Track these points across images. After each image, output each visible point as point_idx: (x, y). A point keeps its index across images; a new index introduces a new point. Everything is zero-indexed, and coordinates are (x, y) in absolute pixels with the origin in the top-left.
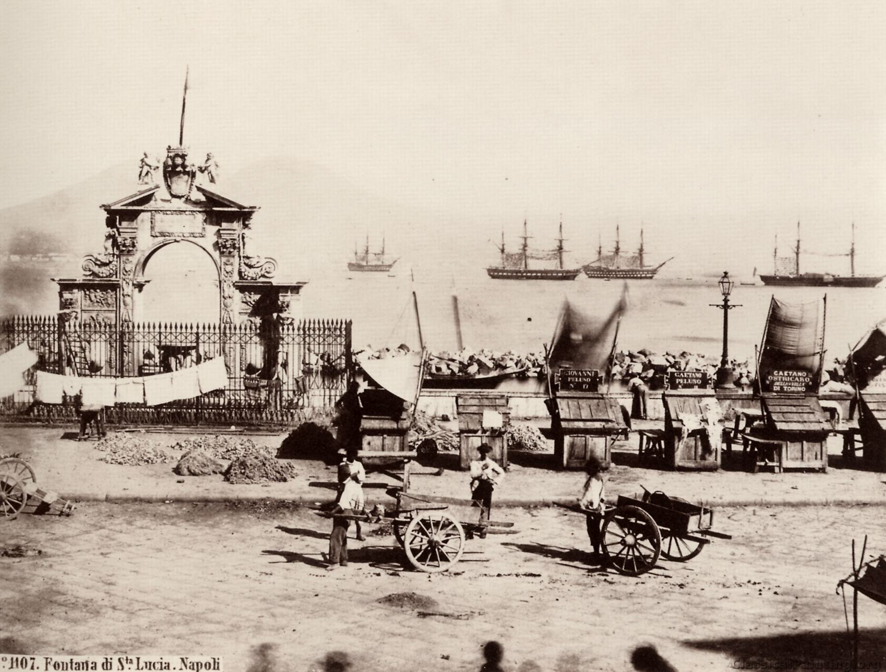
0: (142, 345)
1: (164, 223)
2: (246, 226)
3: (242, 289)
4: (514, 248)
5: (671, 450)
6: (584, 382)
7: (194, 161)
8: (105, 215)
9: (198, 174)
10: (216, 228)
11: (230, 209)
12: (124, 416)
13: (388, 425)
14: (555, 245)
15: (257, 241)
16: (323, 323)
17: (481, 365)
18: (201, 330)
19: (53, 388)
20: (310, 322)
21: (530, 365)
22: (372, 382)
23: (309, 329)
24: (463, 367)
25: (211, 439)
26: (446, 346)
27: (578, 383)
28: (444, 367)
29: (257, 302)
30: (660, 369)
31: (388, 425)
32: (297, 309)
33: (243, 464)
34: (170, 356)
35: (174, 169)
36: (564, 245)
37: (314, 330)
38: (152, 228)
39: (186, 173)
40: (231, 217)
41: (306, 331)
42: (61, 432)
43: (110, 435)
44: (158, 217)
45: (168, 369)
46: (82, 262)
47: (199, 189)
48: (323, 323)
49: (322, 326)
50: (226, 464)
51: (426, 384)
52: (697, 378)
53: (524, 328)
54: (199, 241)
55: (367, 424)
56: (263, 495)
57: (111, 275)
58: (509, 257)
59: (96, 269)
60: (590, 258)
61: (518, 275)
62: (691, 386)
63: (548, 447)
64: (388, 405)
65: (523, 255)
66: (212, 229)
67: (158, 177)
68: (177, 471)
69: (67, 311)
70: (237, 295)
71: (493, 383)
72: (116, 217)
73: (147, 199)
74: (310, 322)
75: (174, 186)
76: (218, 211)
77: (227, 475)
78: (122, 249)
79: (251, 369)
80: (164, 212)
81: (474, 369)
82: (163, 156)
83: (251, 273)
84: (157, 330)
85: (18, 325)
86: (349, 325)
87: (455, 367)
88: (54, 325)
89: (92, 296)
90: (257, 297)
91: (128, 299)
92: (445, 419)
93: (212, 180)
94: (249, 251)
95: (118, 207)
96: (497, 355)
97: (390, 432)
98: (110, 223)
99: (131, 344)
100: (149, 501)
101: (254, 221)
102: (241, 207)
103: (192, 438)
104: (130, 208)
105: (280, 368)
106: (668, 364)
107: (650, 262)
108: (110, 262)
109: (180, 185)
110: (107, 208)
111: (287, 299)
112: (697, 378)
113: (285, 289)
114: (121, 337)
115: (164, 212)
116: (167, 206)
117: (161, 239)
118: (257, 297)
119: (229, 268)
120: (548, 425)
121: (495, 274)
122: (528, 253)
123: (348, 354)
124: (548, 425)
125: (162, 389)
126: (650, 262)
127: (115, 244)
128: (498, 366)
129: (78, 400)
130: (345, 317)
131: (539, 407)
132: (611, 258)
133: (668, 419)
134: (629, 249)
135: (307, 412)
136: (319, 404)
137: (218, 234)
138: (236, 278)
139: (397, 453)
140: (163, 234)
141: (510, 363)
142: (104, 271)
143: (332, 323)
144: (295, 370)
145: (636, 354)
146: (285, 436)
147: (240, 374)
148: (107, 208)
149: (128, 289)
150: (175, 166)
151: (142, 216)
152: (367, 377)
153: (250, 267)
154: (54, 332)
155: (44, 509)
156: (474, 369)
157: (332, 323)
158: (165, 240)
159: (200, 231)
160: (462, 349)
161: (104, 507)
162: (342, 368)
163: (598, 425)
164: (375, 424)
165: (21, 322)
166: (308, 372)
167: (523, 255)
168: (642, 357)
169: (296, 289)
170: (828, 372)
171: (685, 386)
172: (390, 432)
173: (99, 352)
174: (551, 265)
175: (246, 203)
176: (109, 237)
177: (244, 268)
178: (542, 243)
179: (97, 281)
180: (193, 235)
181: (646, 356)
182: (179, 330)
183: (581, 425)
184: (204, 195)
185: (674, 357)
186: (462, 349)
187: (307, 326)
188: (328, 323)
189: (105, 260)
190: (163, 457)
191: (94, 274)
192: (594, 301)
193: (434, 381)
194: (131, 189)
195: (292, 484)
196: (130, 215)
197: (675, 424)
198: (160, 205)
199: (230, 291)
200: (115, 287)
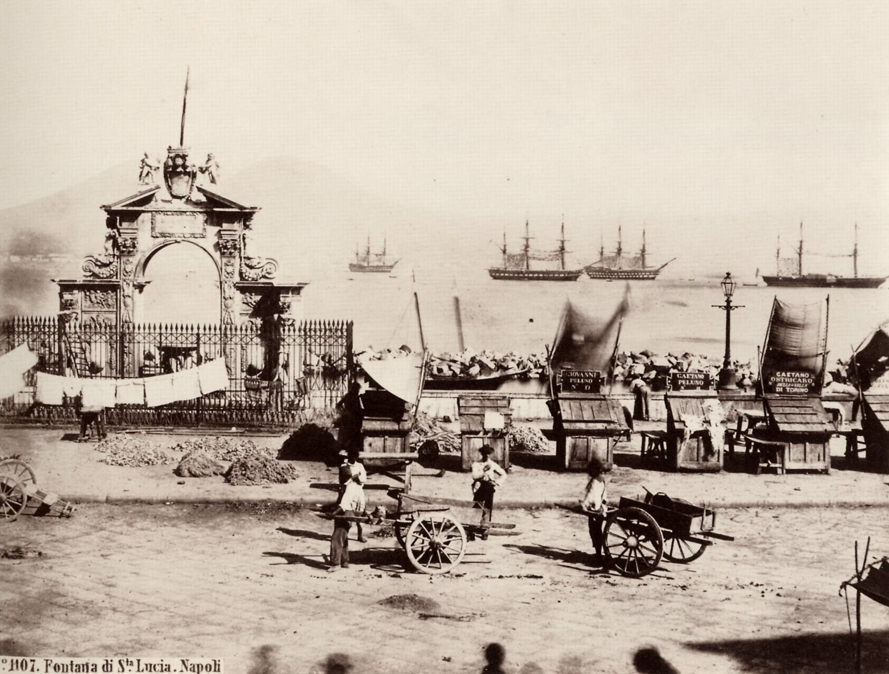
0: (143, 346)
1: (165, 224)
2: (247, 227)
3: (243, 290)
4: (516, 249)
5: (673, 451)
6: (586, 384)
7: (195, 161)
8: (105, 216)
9: (199, 174)
10: (216, 229)
11: (230, 210)
12: (124, 417)
13: (390, 426)
14: (557, 246)
15: (258, 242)
16: (324, 324)
17: (483, 366)
18: (201, 331)
19: (53, 389)
20: (311, 323)
21: (532, 366)
22: (373, 383)
23: (310, 330)
24: (465, 368)
25: (212, 440)
26: (447, 347)
27: (580, 384)
28: (445, 368)
29: (258, 303)
30: (662, 370)
31: (390, 426)
32: (298, 310)
33: (244, 466)
34: (171, 357)
35: (175, 169)
36: (566, 245)
37: (315, 331)
38: (153, 229)
39: (186, 173)
40: (231, 218)
41: (307, 332)
42: (62, 433)
43: (111, 436)
44: (159, 217)
45: (168, 370)
46: (82, 262)
47: (200, 190)
48: (324, 324)
49: (323, 327)
50: (226, 466)
51: (427, 385)
52: (699, 380)
53: (526, 329)
54: (200, 241)
55: (368, 425)
56: (264, 497)
57: (111, 276)
58: (511, 258)
59: (97, 270)
60: (592, 259)
61: (519, 276)
62: (693, 387)
63: (550, 448)
64: (389, 406)
65: (525, 255)
66: (213, 230)
67: (158, 178)
68: (178, 472)
69: (67, 312)
70: (238, 296)
71: (494, 384)
72: (116, 217)
73: (147, 200)
74: (311, 323)
75: (174, 187)
76: (219, 211)
77: (227, 477)
78: (123, 250)
79: (251, 370)
80: (165, 212)
81: (475, 370)
82: (164, 157)
83: (251, 274)
84: (158, 331)
85: (18, 326)
86: (350, 326)
87: (457, 369)
88: (54, 326)
89: (93, 296)
90: (258, 298)
91: (128, 300)
92: (447, 420)
93: (213, 181)
94: (250, 251)
95: (118, 207)
96: (499, 356)
97: (392, 434)
98: (111, 224)
99: (131, 345)
100: (150, 503)
101: (255, 222)
102: (241, 208)
103: (193, 439)
104: (131, 208)
105: (281, 369)
106: (670, 365)
107: (652, 262)
108: (111, 263)
109: (181, 186)
110: (107, 209)
111: (288, 300)
112: (699, 380)
113: (286, 290)
114: (121, 338)
115: (165, 212)
116: (167, 207)
117: (161, 240)
118: (258, 298)
119: (230, 269)
120: (550, 426)
121: (497, 274)
122: (530, 254)
123: (349, 355)
124: (550, 426)
125: (163, 390)
126: (652, 262)
127: (115, 245)
128: (500, 367)
129: (78, 401)
130: (347, 318)
131: (541, 408)
132: (613, 259)
133: (670, 420)
134: (631, 250)
135: (309, 413)
136: (320, 405)
137: (219, 234)
138: (237, 278)
139: (398, 455)
140: (163, 235)
141: (511, 365)
142: (105, 272)
143: (334, 324)
144: (296, 371)
145: (638, 355)
146: (286, 437)
147: (241, 375)
148: (107, 209)
149: (129, 290)
150: (175, 166)
151: (143, 217)
152: (368, 379)
153: (251, 267)
154: (54, 333)
155: (44, 510)
156: (475, 370)
157: (334, 324)
158: (166, 240)
159: (201, 231)
160: (463, 350)
161: (105, 509)
162: (343, 369)
163: (600, 426)
164: (376, 425)
165: (21, 323)
166: (309, 373)
167: (525, 255)
168: (645, 358)
169: (297, 290)
170: (831, 373)
171: (688, 387)
172: (392, 434)
173: (100, 353)
174: (553, 266)
175: (247, 204)
176: (109, 237)
177: (245, 269)
178: (544, 244)
179: (97, 282)
180: (193, 235)
181: (648, 357)
182: (179, 331)
183: (583, 426)
184: (205, 195)
185: (676, 358)
186: (463, 350)
187: (308, 327)
188: (329, 324)
189: (106, 261)
190: (164, 458)
191: (94, 275)
192: (596, 302)
193: (435, 382)
194: (131, 190)
195: (293, 485)
196: (130, 216)
197: (677, 426)
198: (160, 206)
199: (231, 291)
200: (115, 288)
